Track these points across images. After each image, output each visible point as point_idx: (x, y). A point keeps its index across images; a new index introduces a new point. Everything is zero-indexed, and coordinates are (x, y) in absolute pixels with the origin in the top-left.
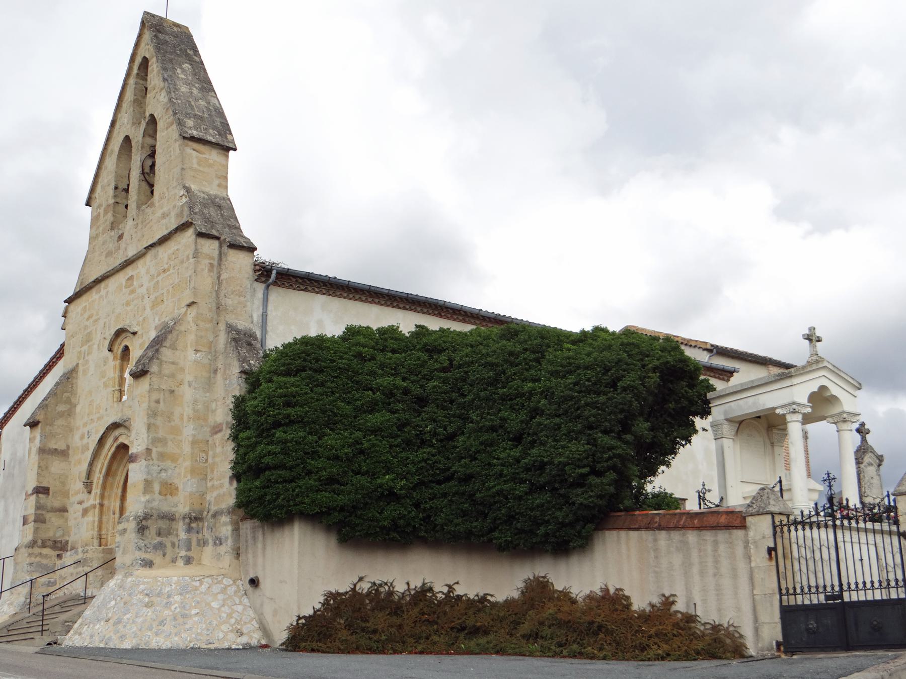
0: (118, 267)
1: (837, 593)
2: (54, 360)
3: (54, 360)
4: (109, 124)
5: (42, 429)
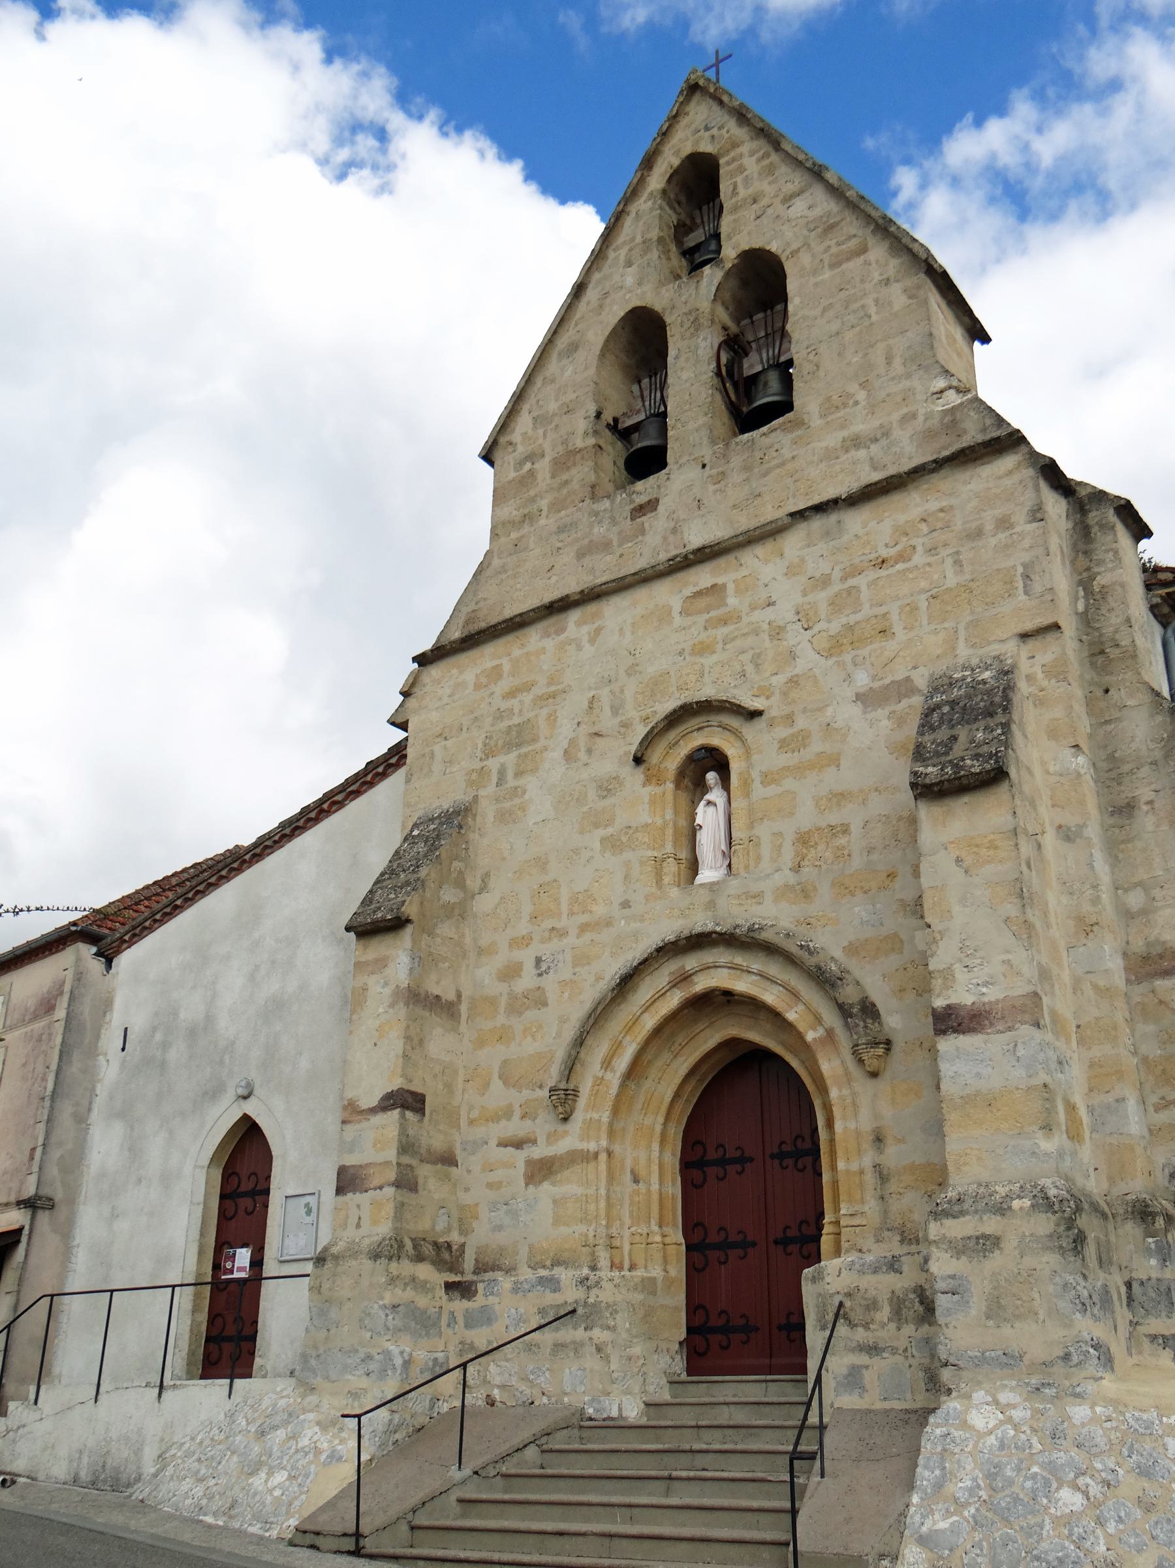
0: (662, 567)
1: (243, 1275)
2: (339, 798)
3: (339, 798)
4: (566, 289)
5: (414, 941)
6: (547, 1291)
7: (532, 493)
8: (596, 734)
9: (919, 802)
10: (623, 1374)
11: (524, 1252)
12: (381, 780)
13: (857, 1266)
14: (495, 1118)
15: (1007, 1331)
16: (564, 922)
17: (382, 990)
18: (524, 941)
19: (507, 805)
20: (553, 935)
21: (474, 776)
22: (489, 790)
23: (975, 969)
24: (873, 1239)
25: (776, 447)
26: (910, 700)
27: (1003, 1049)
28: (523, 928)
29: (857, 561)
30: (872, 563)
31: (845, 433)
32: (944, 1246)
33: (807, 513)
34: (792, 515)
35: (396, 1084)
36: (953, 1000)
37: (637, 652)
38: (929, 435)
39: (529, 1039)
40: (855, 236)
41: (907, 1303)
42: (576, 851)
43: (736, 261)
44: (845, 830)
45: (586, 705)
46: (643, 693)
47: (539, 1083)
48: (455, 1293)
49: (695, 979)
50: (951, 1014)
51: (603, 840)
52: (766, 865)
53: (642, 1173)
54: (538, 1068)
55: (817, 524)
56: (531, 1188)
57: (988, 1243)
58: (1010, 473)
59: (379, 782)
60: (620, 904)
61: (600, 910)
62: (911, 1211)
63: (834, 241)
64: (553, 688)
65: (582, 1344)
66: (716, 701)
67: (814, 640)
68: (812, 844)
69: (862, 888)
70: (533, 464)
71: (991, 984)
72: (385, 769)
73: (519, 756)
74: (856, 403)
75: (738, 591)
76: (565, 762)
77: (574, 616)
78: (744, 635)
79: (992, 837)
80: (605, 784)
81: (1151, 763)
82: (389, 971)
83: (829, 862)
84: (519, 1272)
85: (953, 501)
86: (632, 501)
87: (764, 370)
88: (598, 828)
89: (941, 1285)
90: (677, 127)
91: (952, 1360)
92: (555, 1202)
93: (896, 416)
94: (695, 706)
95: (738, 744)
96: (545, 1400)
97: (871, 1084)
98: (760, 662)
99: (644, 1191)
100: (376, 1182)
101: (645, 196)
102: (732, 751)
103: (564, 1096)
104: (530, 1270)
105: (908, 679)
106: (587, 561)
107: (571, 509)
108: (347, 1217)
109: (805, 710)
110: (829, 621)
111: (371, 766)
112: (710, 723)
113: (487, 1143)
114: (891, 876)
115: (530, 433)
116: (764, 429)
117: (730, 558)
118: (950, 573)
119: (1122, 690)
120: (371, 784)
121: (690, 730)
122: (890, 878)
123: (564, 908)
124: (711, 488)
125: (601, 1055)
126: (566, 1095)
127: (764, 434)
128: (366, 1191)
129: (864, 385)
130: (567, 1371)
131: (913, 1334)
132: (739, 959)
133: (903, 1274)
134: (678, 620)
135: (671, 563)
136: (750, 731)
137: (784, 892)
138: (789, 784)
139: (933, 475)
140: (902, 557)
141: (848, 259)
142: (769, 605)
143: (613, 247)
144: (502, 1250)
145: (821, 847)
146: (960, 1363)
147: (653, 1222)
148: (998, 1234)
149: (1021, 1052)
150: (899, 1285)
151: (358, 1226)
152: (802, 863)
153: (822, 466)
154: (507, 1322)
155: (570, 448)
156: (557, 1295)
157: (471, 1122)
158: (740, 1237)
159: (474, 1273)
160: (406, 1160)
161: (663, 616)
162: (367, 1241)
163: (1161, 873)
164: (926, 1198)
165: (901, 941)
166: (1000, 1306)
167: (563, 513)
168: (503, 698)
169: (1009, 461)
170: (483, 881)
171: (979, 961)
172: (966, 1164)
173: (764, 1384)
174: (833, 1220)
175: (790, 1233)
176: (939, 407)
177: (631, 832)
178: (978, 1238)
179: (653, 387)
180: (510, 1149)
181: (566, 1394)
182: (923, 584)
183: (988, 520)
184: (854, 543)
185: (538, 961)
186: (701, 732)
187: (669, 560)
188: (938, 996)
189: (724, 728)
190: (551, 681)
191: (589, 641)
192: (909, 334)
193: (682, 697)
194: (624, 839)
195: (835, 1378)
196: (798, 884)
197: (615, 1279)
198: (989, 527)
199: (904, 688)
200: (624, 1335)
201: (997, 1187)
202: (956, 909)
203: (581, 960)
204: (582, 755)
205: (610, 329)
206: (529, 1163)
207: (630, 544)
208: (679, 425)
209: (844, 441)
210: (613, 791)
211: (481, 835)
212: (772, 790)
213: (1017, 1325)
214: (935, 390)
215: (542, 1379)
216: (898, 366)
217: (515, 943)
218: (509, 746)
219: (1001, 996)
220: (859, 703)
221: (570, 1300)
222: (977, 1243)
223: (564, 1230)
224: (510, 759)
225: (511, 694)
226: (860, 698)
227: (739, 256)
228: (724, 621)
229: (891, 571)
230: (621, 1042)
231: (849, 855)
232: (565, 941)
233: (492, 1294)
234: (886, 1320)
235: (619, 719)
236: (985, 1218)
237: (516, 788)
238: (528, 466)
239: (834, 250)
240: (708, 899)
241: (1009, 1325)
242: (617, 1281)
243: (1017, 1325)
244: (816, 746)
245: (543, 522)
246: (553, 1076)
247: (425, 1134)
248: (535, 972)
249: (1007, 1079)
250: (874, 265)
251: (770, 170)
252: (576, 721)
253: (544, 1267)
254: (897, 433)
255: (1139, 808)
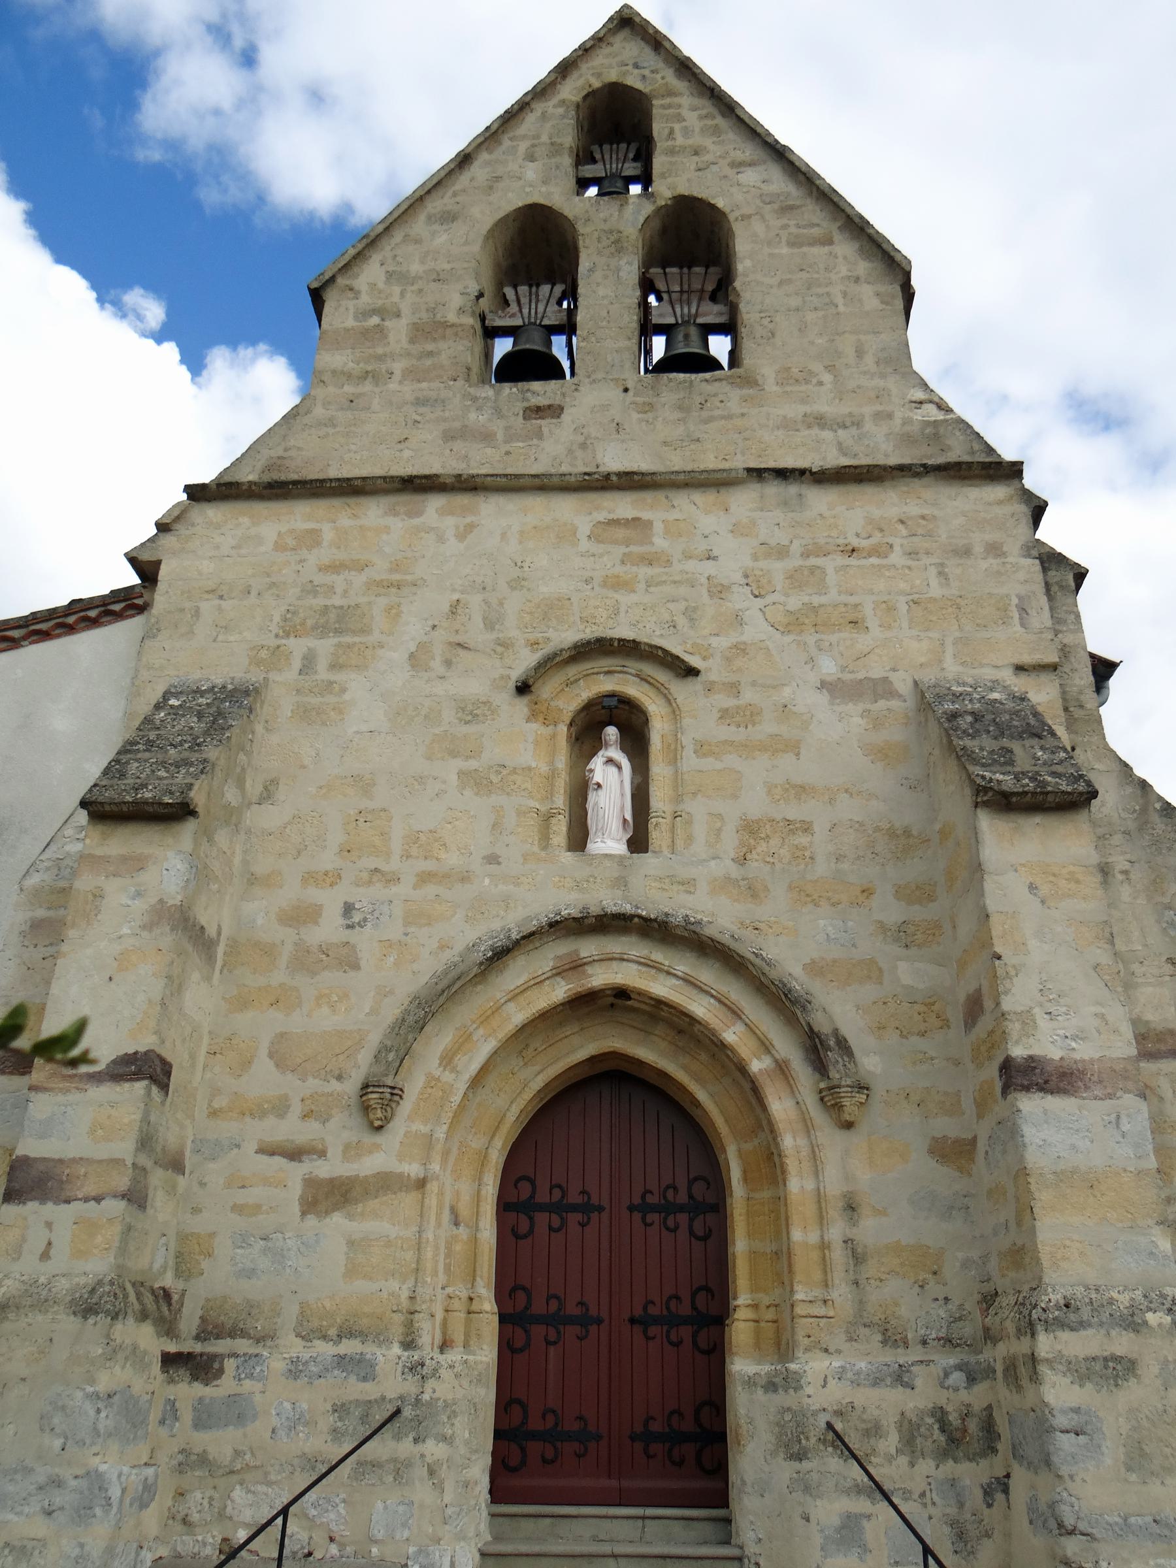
0: (573, 479)
6: (353, 1379)
7: (380, 351)
8: (459, 644)
9: (979, 810)
10: (458, 1509)
11: (291, 1312)
12: (88, 628)
13: (849, 1375)
14: (258, 1111)
15: (1155, 1488)
16: (394, 864)
17: (130, 903)
18: (333, 878)
19: (315, 701)
20: (375, 879)
21: (264, 654)
22: (290, 675)
23: (1059, 1018)
24: (843, 1337)
25: (721, 397)
26: (889, 703)
27: (1103, 1119)
28: (328, 860)
29: (822, 541)
30: (841, 549)
31: (807, 409)
32: (1060, 1367)
33: (766, 474)
34: (749, 470)
35: (144, 1043)
36: (1036, 1051)
37: (526, 565)
38: (907, 439)
39: (325, 1010)
40: (818, 225)
41: (922, 1430)
42: (421, 779)
43: (669, 202)
44: (807, 828)
45: (446, 608)
46: (531, 613)
47: (337, 1072)
48: (182, 1372)
49: (589, 970)
50: (1035, 1068)
51: (461, 774)
52: (699, 848)
53: (465, 1211)
54: (338, 1051)
55: (773, 489)
56: (312, 1221)
57: (1119, 1367)
58: (1000, 503)
59: (83, 629)
60: (483, 858)
61: (452, 860)
62: (896, 1305)
63: (795, 222)
64: (396, 577)
65: (408, 1464)
66: (646, 644)
67: (767, 610)
68: (762, 835)
69: (829, 899)
70: (383, 320)
71: (1081, 1039)
72: (100, 616)
73: (339, 645)
74: (821, 383)
75: (667, 532)
76: (409, 668)
77: (435, 503)
78: (675, 582)
79: (1072, 868)
80: (470, 707)
81: (1124, 832)
82: (148, 878)
83: (785, 860)
84: (280, 1342)
85: (936, 513)
86: (525, 399)
87: (677, 323)
88: (455, 757)
89: (1061, 1421)
90: (598, 51)
91: (1082, 1526)
92: (351, 1243)
93: (868, 410)
94: (616, 644)
95: (661, 701)
96: (334, 1550)
97: (840, 1136)
98: (695, 616)
99: (465, 1237)
100: (90, 1189)
101: (555, 100)
102: (654, 707)
103: (388, 1096)
104: (299, 1340)
105: (885, 680)
106: (459, 446)
107: (436, 384)
108: (24, 1239)
109: (754, 684)
110: (787, 595)
111: (78, 606)
112: (625, 669)
113: (238, 1146)
114: (867, 892)
115: (381, 285)
116: (702, 375)
117: (660, 495)
118: (934, 582)
119: (1089, 752)
120: (71, 629)
121: (596, 670)
122: (865, 894)
123: (397, 846)
124: (635, 416)
125: (441, 1047)
126: (392, 1094)
127: (706, 381)
128: (68, 1202)
129: (829, 368)
130: (379, 1505)
131: (932, 1472)
132: (659, 955)
133: (916, 1390)
134: (585, 545)
135: (586, 477)
136: (681, 690)
137: (724, 884)
138: (732, 760)
139: (916, 480)
140: (875, 551)
141: (811, 244)
142: (708, 559)
143: (511, 134)
144: (251, 1308)
145: (775, 842)
146: (1094, 1531)
147: (480, 1283)
148: (1134, 1356)
149: (1125, 1127)
150: (911, 1405)
151: (45, 1256)
152: (749, 856)
153: (780, 433)
154: (275, 1422)
155: (438, 317)
156: (368, 1386)
157: (214, 1114)
158: (554, 1306)
159: (197, 1338)
160: (144, 1160)
161: (566, 535)
162: (63, 1285)
163: (1140, 948)
164: (916, 1289)
165: (880, 970)
166: (1143, 1454)
167: (424, 385)
168: (320, 570)
169: (998, 491)
170: (266, 788)
171: (1064, 1009)
172: (1064, 1259)
173: (640, 1523)
174: (750, 1302)
175: (653, 1311)
176: (918, 415)
177: (505, 772)
178: (1106, 1359)
179: (534, 297)
180: (278, 1160)
181: (376, 1542)
182: (903, 585)
183: (978, 540)
184: (819, 521)
185: (348, 909)
186: (609, 677)
187: (585, 474)
188: (1017, 1042)
189: (642, 679)
190: (396, 567)
191: (456, 536)
192: (883, 336)
193: (588, 630)
194: (495, 779)
195: (822, 1531)
196: (743, 879)
197: (457, 1365)
198: (978, 549)
199: (881, 688)
200: (463, 1450)
201: (1112, 1294)
202: (1033, 943)
203: (415, 917)
204: (437, 665)
205: (501, 214)
206: (310, 1182)
207: (521, 444)
208: (593, 339)
209: (805, 415)
210: (481, 718)
211: (267, 730)
212: (709, 763)
213: (1168, 1481)
214: (914, 399)
215: (332, 1516)
216: (869, 360)
217: (310, 878)
218: (322, 630)
219: (1097, 1056)
220: (824, 690)
221: (391, 1395)
222: (1106, 1367)
223: (362, 1286)
224: (325, 647)
225: (335, 568)
226: (824, 685)
227: (674, 197)
228: (649, 560)
229: (863, 562)
230: (471, 1034)
231: (812, 858)
232: (394, 889)
233: (251, 1376)
234: (893, 1451)
235: (494, 636)
236: (1113, 1333)
237: (331, 683)
238: (375, 320)
239: (793, 230)
240: (616, 875)
241: (1158, 1483)
242: (458, 1368)
243: (1168, 1481)
244: (768, 727)
245: (393, 386)
246: (361, 1066)
247: (164, 1123)
248: (341, 921)
249: (1112, 1158)
250: (840, 259)
251: (716, 131)
252: (430, 623)
253: (324, 1337)
254: (869, 426)
255: (1114, 876)
